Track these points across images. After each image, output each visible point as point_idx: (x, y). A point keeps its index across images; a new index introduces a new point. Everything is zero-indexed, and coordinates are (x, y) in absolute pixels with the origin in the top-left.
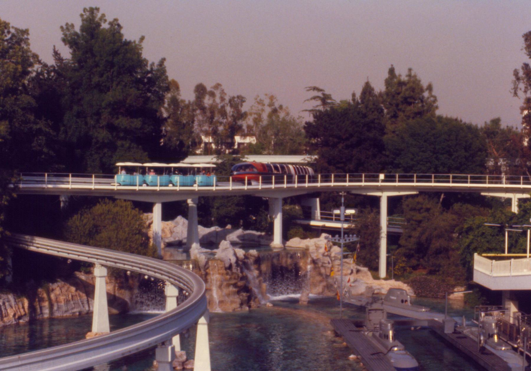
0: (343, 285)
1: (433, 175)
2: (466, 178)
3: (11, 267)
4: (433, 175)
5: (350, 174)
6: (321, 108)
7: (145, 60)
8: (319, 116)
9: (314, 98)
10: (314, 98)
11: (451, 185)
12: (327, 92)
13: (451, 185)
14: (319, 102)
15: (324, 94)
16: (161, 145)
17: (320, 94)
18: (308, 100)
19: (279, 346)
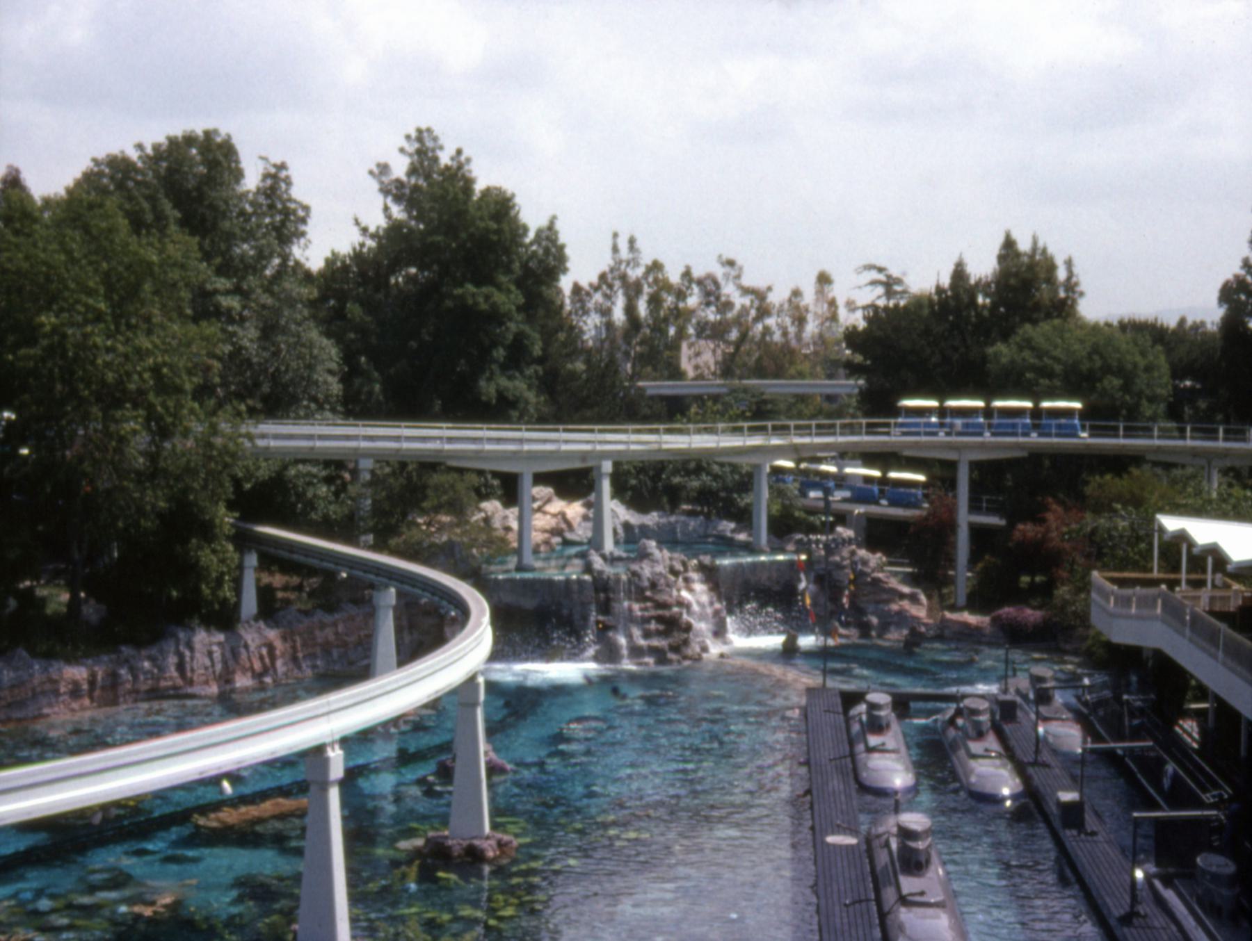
0: (982, 648)
1: (1121, 426)
2: (1116, 429)
3: (437, 781)
4: (1121, 426)
5: (1093, 423)
6: (881, 303)
7: (327, 261)
8: (876, 316)
9: (874, 283)
10: (874, 283)
11: (1122, 441)
12: (895, 272)
13: (1122, 441)
14: (880, 290)
15: (889, 277)
16: (13, 417)
17: (882, 277)
18: (860, 287)
19: (335, 624)
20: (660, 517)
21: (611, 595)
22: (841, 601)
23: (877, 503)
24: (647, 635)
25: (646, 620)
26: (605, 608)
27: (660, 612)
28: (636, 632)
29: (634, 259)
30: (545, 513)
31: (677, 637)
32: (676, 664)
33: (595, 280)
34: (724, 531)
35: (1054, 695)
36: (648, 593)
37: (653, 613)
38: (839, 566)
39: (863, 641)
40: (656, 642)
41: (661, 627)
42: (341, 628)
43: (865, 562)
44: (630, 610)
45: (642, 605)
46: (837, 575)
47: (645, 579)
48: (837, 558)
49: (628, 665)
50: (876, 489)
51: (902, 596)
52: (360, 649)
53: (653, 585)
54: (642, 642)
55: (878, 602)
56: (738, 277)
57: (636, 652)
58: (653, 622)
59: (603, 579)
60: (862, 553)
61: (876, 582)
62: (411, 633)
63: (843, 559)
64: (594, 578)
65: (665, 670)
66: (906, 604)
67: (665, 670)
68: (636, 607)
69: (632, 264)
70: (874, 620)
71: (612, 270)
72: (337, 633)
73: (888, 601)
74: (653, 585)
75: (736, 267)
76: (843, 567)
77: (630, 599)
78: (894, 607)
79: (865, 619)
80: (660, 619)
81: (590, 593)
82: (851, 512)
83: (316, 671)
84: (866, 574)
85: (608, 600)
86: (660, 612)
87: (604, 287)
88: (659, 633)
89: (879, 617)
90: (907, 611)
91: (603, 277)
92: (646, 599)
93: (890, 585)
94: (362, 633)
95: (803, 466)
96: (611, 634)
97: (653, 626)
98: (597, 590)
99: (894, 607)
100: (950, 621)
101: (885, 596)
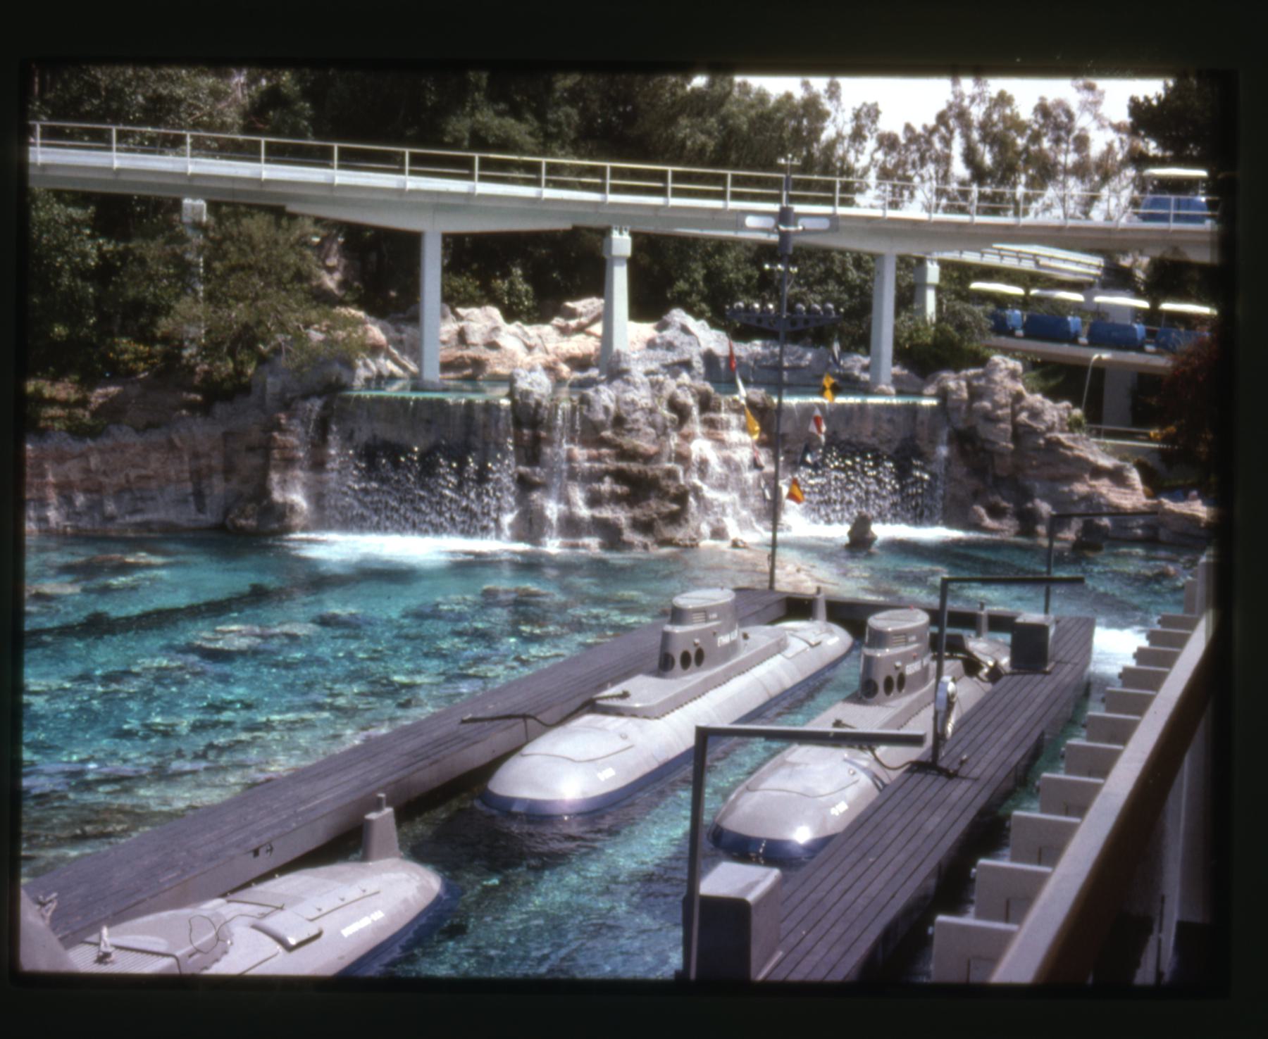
19: (83, 456)
20: (764, 347)
21: (543, 434)
22: (828, 428)
23: (1140, 349)
24: (594, 500)
25: (598, 477)
26: (531, 453)
27: (623, 465)
28: (578, 495)
29: (980, 94)
30: (589, 334)
31: (654, 507)
32: (640, 550)
33: (931, 122)
34: (851, 368)
35: (293, 501)
36: (607, 434)
37: (611, 464)
38: (990, 418)
39: (1020, 540)
40: (606, 513)
41: (619, 489)
42: (94, 461)
43: (1035, 414)
44: (570, 459)
45: (594, 452)
46: (984, 430)
47: (598, 408)
48: (987, 404)
49: (553, 546)
50: (1140, 328)
51: (1098, 472)
52: (127, 496)
53: (619, 422)
54: (584, 512)
55: (1054, 479)
56: (1096, 103)
57: (571, 526)
58: (607, 479)
59: (527, 405)
60: (1036, 399)
61: (1054, 445)
62: (227, 480)
63: (997, 405)
64: (514, 403)
65: (615, 557)
66: (1103, 486)
67: (615, 557)
68: (580, 453)
69: (978, 100)
70: (1045, 508)
71: (950, 107)
72: (87, 471)
73: (1070, 479)
74: (619, 422)
75: (1096, 93)
76: (997, 420)
77: (571, 440)
78: (1080, 488)
79: (1029, 505)
80: (619, 476)
81: (505, 422)
82: (1089, 359)
83: (44, 526)
84: (1034, 432)
85: (537, 441)
86: (623, 465)
87: (943, 130)
88: (616, 499)
89: (1054, 504)
90: (1101, 495)
91: (942, 118)
92: (603, 442)
93: (1077, 452)
94: (133, 474)
95: (1034, 292)
96: (535, 496)
97: (606, 486)
98: (518, 423)
99: (1080, 488)
100: (1172, 513)
101: (1064, 470)
